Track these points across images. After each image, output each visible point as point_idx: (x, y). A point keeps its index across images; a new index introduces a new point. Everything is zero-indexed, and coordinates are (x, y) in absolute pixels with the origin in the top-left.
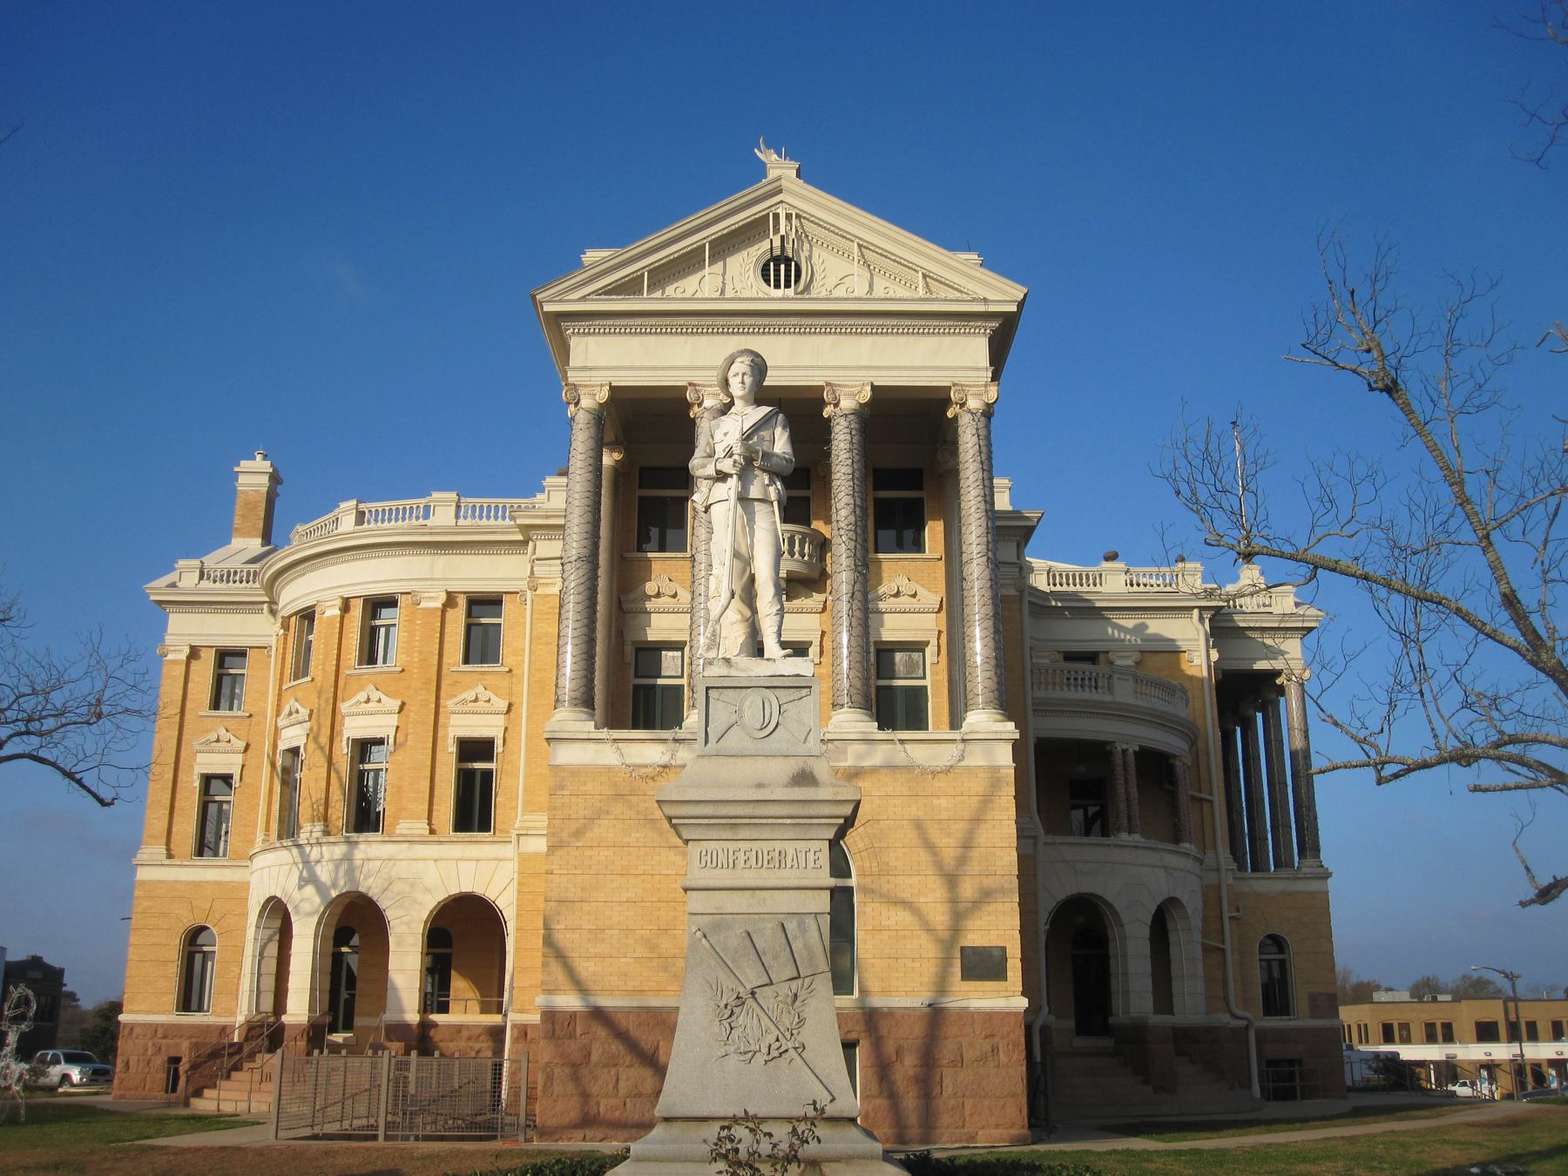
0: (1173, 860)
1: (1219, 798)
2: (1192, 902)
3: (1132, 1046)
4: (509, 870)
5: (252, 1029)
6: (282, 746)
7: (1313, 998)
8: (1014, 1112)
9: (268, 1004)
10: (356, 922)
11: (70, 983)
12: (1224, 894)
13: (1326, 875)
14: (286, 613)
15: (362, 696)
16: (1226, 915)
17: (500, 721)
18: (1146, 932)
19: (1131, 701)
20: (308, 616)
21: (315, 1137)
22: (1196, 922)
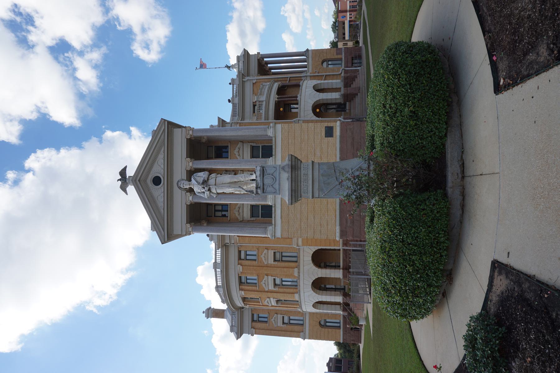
0: (304, 87)
1: (289, 76)
2: (315, 82)
3: (349, 97)
4: (306, 248)
5: (344, 310)
6: (276, 305)
7: (337, 54)
8: (337, 271)
9: (338, 306)
10: (319, 285)
11: (332, 356)
12: (312, 75)
13: (308, 50)
14: (243, 305)
15: (264, 285)
16: (317, 74)
17: (270, 251)
18: (321, 94)
19: (265, 96)
20: (244, 299)
21: (370, 293)
22: (319, 82)
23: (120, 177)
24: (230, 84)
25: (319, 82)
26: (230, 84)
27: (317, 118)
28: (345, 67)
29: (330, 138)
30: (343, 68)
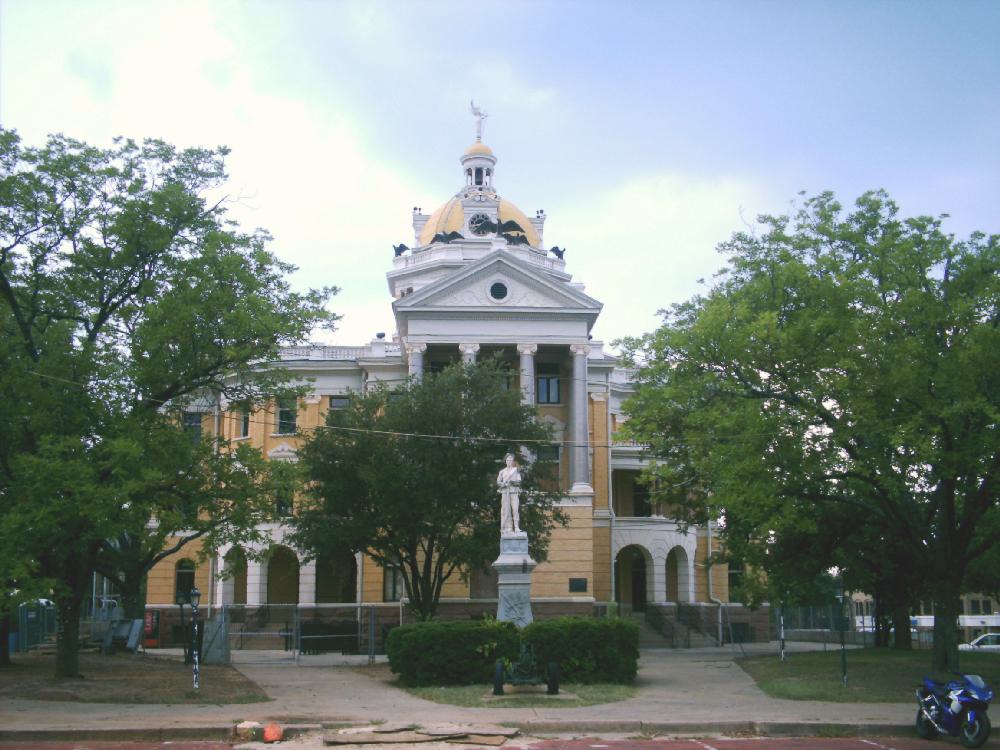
22: (691, 556)
23: (503, 222)
25: (691, 556)
27: (614, 555)
28: (723, 608)
29: (567, 587)
30: (723, 604)
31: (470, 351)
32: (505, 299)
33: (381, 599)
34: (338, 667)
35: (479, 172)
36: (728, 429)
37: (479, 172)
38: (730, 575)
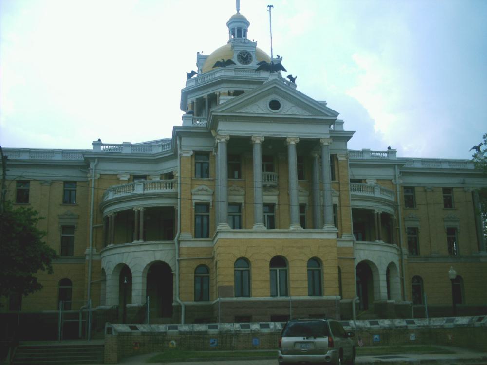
24: (389, 148)
26: (389, 148)
31: (258, 141)
32: (278, 111)
33: (194, 300)
34: (368, 244)
35: (239, 30)
36: (145, 333)
37: (239, 30)
38: (448, 238)
